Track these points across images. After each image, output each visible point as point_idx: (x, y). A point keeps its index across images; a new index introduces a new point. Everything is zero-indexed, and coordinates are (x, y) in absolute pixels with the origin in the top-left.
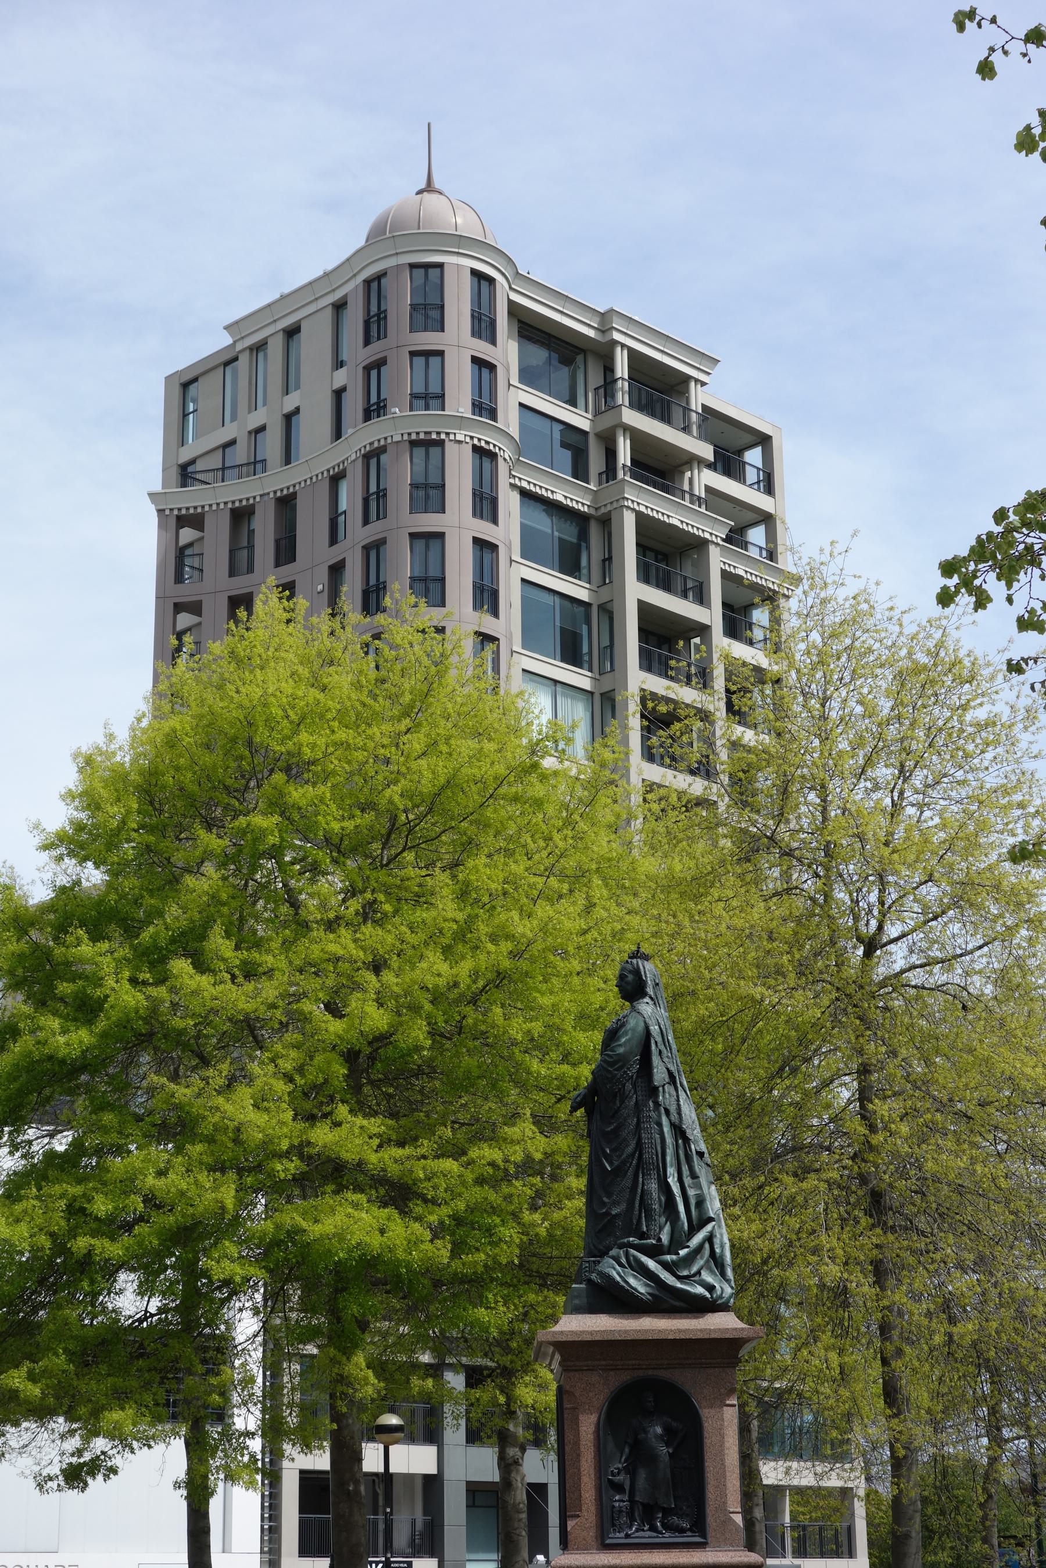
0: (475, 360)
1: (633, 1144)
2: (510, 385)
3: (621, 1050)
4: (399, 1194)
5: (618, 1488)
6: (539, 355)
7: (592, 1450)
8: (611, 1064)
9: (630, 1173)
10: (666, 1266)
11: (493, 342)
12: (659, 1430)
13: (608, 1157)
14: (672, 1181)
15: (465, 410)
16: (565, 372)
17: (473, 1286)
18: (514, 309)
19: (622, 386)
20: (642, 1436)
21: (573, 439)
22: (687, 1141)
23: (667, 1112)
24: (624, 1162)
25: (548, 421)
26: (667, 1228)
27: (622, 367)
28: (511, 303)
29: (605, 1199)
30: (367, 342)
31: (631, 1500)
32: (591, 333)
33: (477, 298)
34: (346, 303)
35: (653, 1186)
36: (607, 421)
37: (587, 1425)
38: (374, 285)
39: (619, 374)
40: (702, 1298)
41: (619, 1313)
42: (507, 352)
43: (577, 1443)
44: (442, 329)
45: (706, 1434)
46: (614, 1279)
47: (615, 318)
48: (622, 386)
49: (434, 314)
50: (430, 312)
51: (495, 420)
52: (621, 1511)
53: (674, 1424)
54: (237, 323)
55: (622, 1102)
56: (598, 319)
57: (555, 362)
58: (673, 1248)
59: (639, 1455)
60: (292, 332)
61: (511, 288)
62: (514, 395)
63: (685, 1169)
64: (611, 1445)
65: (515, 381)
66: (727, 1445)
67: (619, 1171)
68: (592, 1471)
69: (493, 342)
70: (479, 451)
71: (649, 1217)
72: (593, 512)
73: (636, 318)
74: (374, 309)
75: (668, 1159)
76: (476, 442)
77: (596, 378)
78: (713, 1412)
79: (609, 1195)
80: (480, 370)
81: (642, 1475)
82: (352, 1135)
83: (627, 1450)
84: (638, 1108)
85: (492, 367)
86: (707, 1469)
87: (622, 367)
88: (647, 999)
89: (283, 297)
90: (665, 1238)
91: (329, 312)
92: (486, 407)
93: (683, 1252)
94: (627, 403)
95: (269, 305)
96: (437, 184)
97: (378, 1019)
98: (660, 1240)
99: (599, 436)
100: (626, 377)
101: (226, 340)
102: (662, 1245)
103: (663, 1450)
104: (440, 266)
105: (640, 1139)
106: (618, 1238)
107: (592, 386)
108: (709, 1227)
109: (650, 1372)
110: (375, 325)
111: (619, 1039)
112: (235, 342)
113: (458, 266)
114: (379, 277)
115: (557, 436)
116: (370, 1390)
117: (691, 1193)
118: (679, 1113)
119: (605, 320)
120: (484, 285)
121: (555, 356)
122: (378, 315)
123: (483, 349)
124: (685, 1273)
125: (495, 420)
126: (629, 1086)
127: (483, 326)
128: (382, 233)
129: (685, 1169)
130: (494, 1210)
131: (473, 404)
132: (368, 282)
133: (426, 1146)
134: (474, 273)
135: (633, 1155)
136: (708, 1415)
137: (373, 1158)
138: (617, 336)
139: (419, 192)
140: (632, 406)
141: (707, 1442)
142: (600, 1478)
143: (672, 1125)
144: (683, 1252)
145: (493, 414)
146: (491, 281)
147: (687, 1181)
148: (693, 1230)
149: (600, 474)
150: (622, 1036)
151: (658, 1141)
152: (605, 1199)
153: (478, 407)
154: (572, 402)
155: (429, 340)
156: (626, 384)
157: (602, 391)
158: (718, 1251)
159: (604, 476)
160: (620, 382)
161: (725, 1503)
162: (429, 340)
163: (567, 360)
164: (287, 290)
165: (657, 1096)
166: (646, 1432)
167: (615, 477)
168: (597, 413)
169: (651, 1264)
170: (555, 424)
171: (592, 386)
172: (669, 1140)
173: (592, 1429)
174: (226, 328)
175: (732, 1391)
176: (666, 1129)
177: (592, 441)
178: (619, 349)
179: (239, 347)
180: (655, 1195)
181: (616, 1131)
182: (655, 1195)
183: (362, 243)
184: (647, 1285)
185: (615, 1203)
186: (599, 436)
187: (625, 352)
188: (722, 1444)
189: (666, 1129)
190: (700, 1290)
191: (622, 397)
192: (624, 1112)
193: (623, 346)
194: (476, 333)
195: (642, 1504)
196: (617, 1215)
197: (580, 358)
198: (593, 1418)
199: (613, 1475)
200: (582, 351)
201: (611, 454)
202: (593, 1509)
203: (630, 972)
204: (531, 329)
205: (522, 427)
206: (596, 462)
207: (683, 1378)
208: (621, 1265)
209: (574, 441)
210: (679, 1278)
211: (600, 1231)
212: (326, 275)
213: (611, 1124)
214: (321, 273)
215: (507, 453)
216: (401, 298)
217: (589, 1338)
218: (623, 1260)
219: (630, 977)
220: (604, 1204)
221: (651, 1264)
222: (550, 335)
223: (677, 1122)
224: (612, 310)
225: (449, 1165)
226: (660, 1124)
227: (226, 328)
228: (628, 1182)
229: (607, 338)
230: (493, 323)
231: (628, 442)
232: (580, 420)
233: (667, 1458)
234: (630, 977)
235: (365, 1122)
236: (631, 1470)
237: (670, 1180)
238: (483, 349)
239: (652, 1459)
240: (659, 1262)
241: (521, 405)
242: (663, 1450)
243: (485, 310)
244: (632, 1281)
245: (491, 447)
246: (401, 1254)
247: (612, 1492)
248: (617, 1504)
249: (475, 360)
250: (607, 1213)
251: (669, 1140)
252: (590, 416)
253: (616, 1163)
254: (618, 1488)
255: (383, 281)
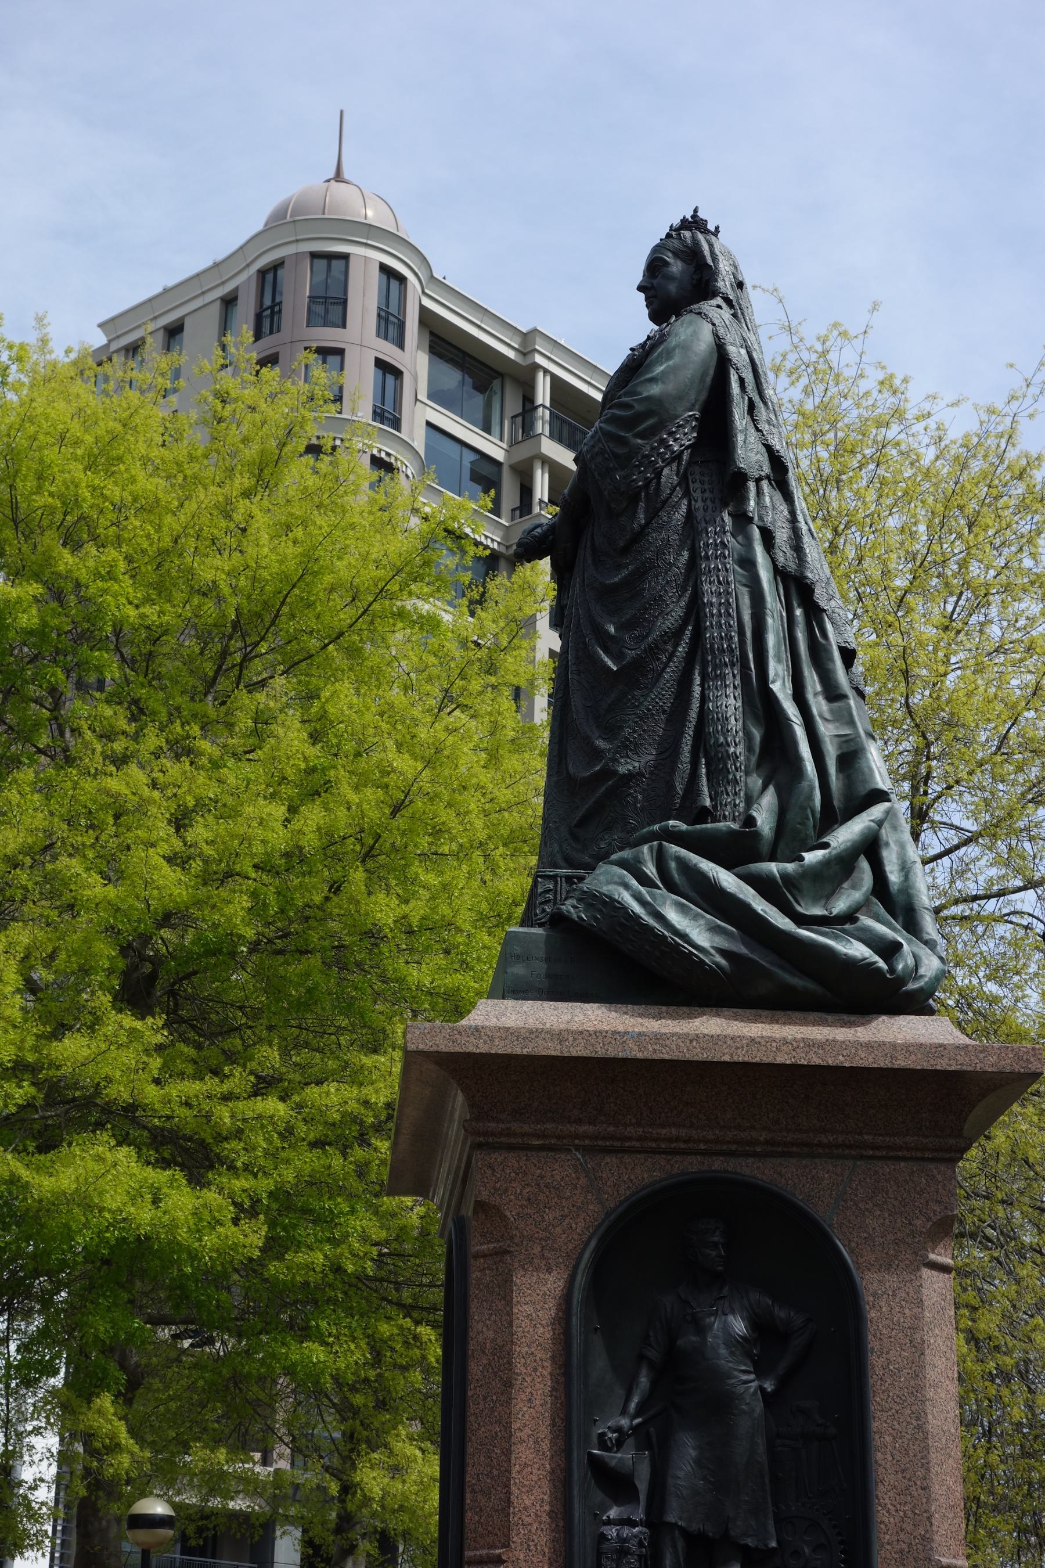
0: (380, 363)
1: (676, 610)
2: (417, 400)
3: (655, 390)
4: (191, 1153)
5: (616, 1484)
6: (452, 377)
7: (546, 1370)
8: (629, 423)
9: (671, 673)
10: (764, 886)
11: (401, 345)
12: (739, 1326)
13: (607, 643)
14: (781, 688)
15: (364, 414)
16: (479, 399)
17: (293, 1309)
18: (426, 317)
19: (543, 415)
20: (688, 1340)
21: (486, 470)
22: (814, 613)
23: (768, 538)
24: (654, 651)
25: (457, 447)
26: (769, 800)
27: (543, 394)
28: (423, 309)
29: (601, 744)
30: (258, 336)
31: (655, 1522)
32: (511, 354)
33: (386, 296)
34: (236, 298)
35: (730, 703)
36: (523, 452)
37: (535, 1304)
38: (270, 275)
39: (539, 401)
40: (865, 968)
41: (635, 1003)
42: (416, 362)
43: (503, 1356)
44: (344, 326)
45: (872, 1343)
46: (624, 909)
47: (538, 340)
48: (543, 415)
49: (335, 311)
50: (331, 305)
51: (399, 430)
52: (622, 1552)
53: (781, 1313)
54: (112, 320)
55: (653, 514)
56: (519, 340)
57: (468, 388)
58: (789, 839)
59: (681, 1393)
60: (174, 332)
61: (423, 292)
62: (421, 413)
63: (812, 682)
64: (600, 1363)
65: (423, 396)
66: (931, 1374)
67: (636, 674)
68: (544, 1431)
69: (401, 345)
70: (377, 462)
71: (719, 774)
72: (503, 550)
73: (562, 342)
74: (268, 302)
75: (771, 640)
76: (375, 452)
77: (513, 405)
78: (892, 1280)
79: (611, 731)
80: (384, 375)
81: (687, 1452)
82: (119, 1051)
83: (644, 1381)
84: (692, 527)
85: (397, 373)
86: (877, 1440)
87: (543, 394)
88: (719, 301)
89: (166, 291)
90: (764, 817)
91: (216, 309)
92: (388, 415)
93: (812, 857)
94: (547, 433)
95: (150, 300)
96: (346, 174)
97: (173, 885)
98: (750, 821)
99: (513, 468)
100: (548, 404)
101: (99, 339)
102: (757, 835)
103: (747, 1384)
104: (345, 257)
105: (696, 596)
106: (635, 829)
107: (509, 412)
108: (877, 811)
109: (718, 1164)
110: (268, 319)
111: (650, 368)
112: (110, 341)
113: (366, 258)
114: (277, 266)
115: (466, 465)
116: (125, 1460)
117: (826, 731)
118: (797, 547)
119: (528, 339)
120: (394, 284)
121: (469, 380)
122: (272, 307)
123: (389, 352)
124: (818, 911)
125: (399, 430)
126: (669, 475)
127: (390, 325)
128: (284, 220)
129: (812, 682)
130: (335, 1190)
131: (374, 412)
132: (262, 273)
133: (238, 1079)
134: (384, 269)
135: (676, 635)
136: (880, 1294)
137: (152, 1093)
138: (539, 359)
139: (328, 181)
140: (551, 437)
141: (876, 1362)
142: (567, 1452)
143: (779, 572)
144: (812, 857)
145: (396, 424)
146: (402, 279)
147: (818, 705)
148: (832, 817)
149: (513, 510)
150: (658, 361)
151: (746, 601)
152: (601, 744)
153: (379, 415)
154: (487, 428)
155: (330, 336)
156: (547, 412)
157: (519, 420)
158: (894, 877)
159: (518, 513)
160: (541, 409)
161: (926, 1540)
162: (330, 336)
163: (482, 387)
164: (171, 283)
165: (744, 499)
166: (702, 1330)
167: (530, 512)
168: (513, 443)
169: (728, 880)
170: (465, 451)
171: (509, 412)
172: (773, 604)
173: (548, 1311)
174: (100, 326)
175: (944, 1228)
176: (765, 574)
177: (506, 473)
178: (541, 374)
179: (114, 347)
180: (734, 724)
181: (632, 585)
182: (734, 724)
183: (259, 227)
184: (714, 929)
185: (629, 747)
186: (513, 468)
187: (548, 379)
188: (917, 1370)
189: (765, 574)
190: (858, 950)
191: (542, 425)
192: (657, 538)
193: (546, 371)
194: (383, 332)
195: (683, 1531)
196: (630, 776)
197: (496, 384)
198: (554, 1283)
199: (603, 1444)
200: (501, 375)
201: (526, 491)
202: (543, 1540)
203: (676, 254)
204: (446, 344)
205: (428, 447)
206: (510, 497)
207: (810, 1183)
208: (645, 880)
209: (485, 474)
210: (801, 920)
211: (583, 822)
212: (216, 265)
213: (619, 567)
214: (210, 263)
215: (408, 467)
216: (299, 289)
217: (552, 1049)
218: (650, 870)
219: (676, 267)
220: (597, 754)
221: (728, 880)
222: (465, 354)
223: (792, 566)
224: (535, 331)
225: (273, 1106)
226: (748, 563)
227: (100, 326)
228: (663, 695)
229: (529, 362)
230: (401, 326)
231: (546, 476)
232: (495, 449)
233: (759, 1407)
234: (676, 267)
235: (138, 1024)
236: (653, 1436)
237: (776, 687)
238: (389, 352)
239: (719, 1404)
240: (750, 879)
241: (429, 424)
242: (747, 1384)
243: (393, 309)
244: (673, 916)
245: (393, 460)
246: (182, 1235)
247: (599, 1496)
248: (612, 1532)
249: (380, 363)
250: (608, 773)
251: (773, 604)
252: (505, 446)
253: (631, 654)
254: (616, 1484)
255: (280, 272)
